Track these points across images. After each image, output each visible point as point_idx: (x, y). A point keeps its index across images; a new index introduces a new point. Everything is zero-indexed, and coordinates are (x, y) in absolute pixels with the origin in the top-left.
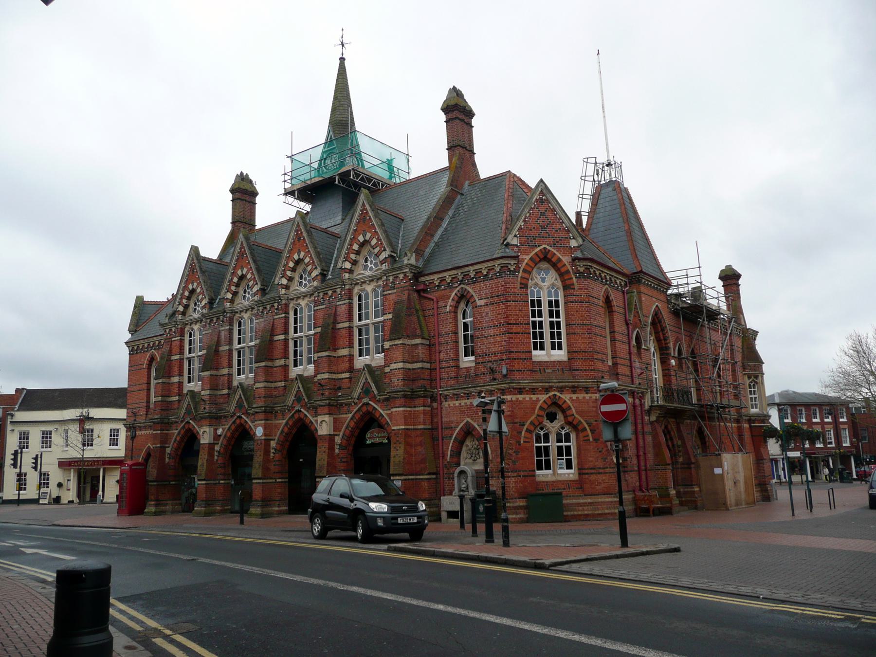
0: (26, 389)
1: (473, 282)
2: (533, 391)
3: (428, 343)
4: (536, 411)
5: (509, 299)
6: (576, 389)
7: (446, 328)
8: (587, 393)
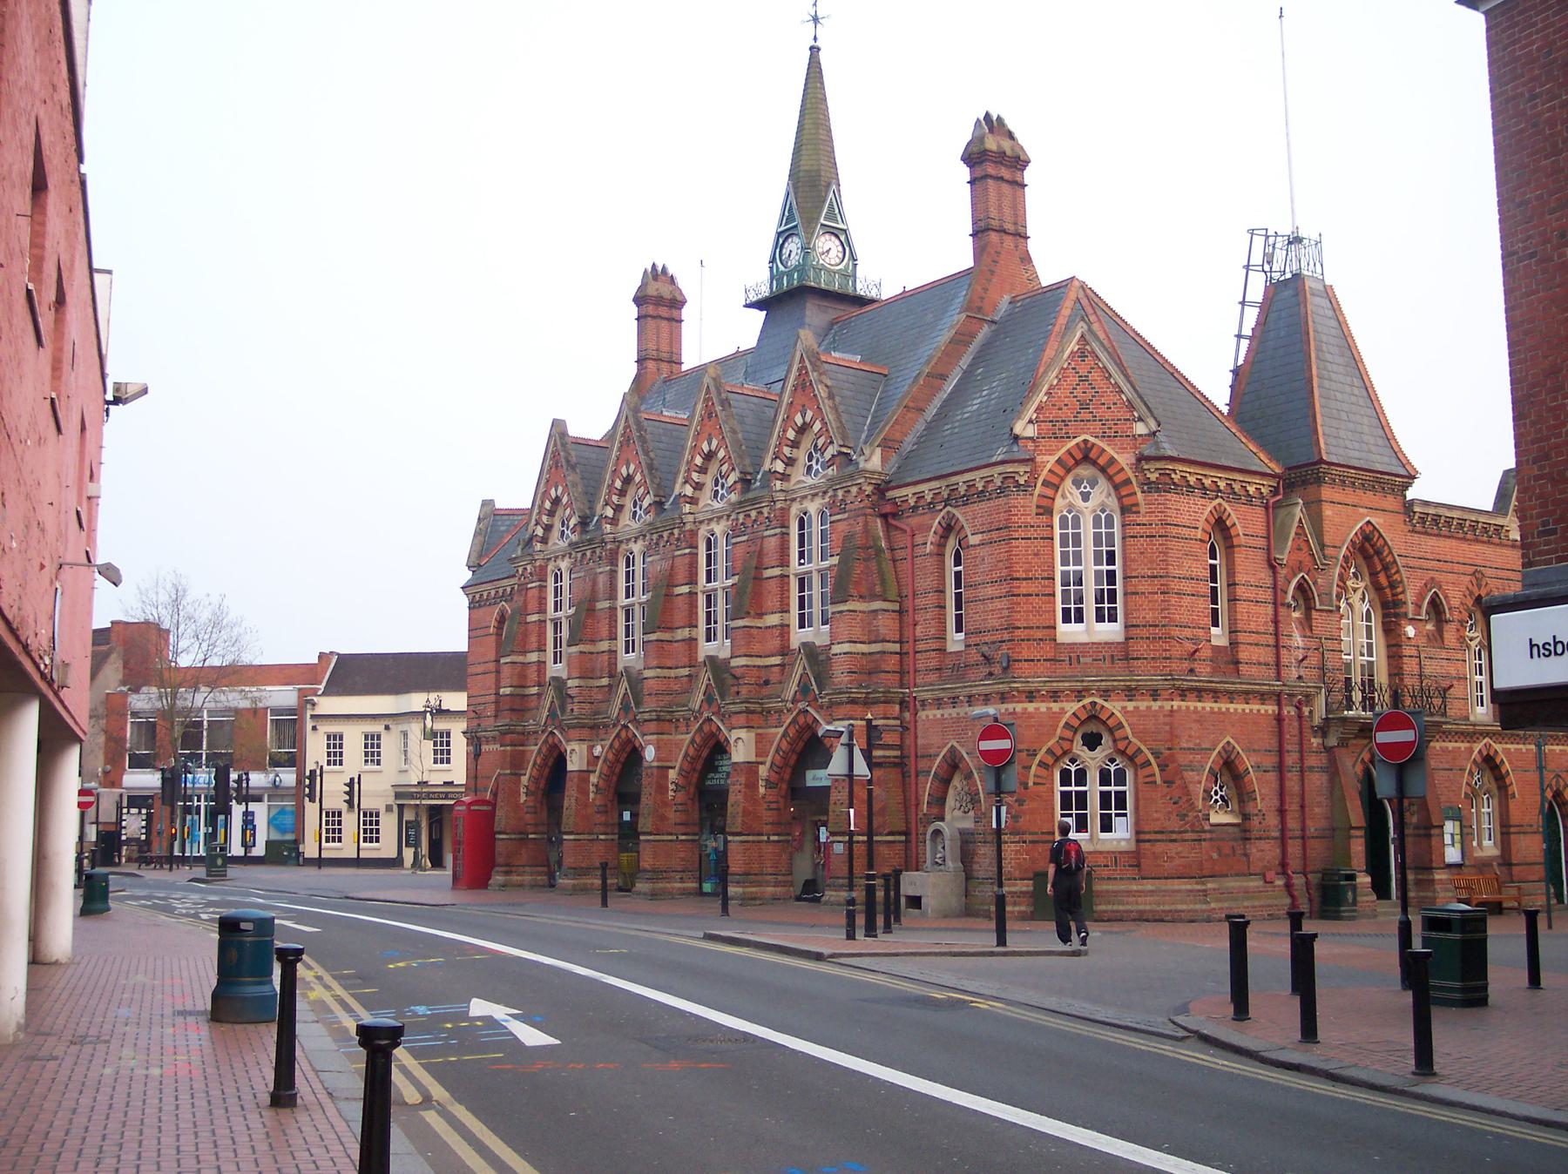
0: (338, 654)
1: (966, 500)
2: (1055, 695)
3: (898, 608)
4: (1059, 730)
5: (1016, 535)
6: (1133, 692)
7: (925, 582)
8: (1155, 700)
